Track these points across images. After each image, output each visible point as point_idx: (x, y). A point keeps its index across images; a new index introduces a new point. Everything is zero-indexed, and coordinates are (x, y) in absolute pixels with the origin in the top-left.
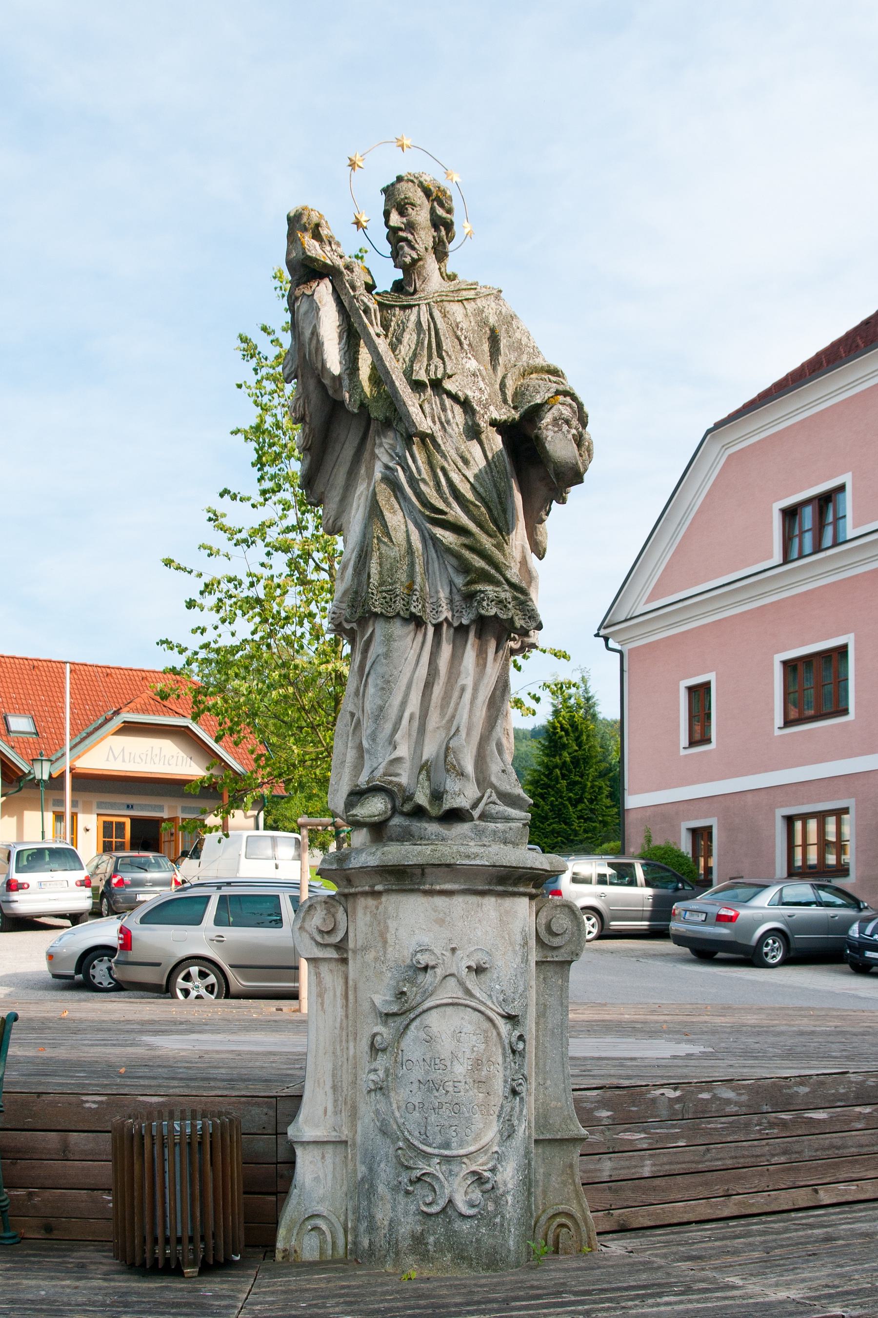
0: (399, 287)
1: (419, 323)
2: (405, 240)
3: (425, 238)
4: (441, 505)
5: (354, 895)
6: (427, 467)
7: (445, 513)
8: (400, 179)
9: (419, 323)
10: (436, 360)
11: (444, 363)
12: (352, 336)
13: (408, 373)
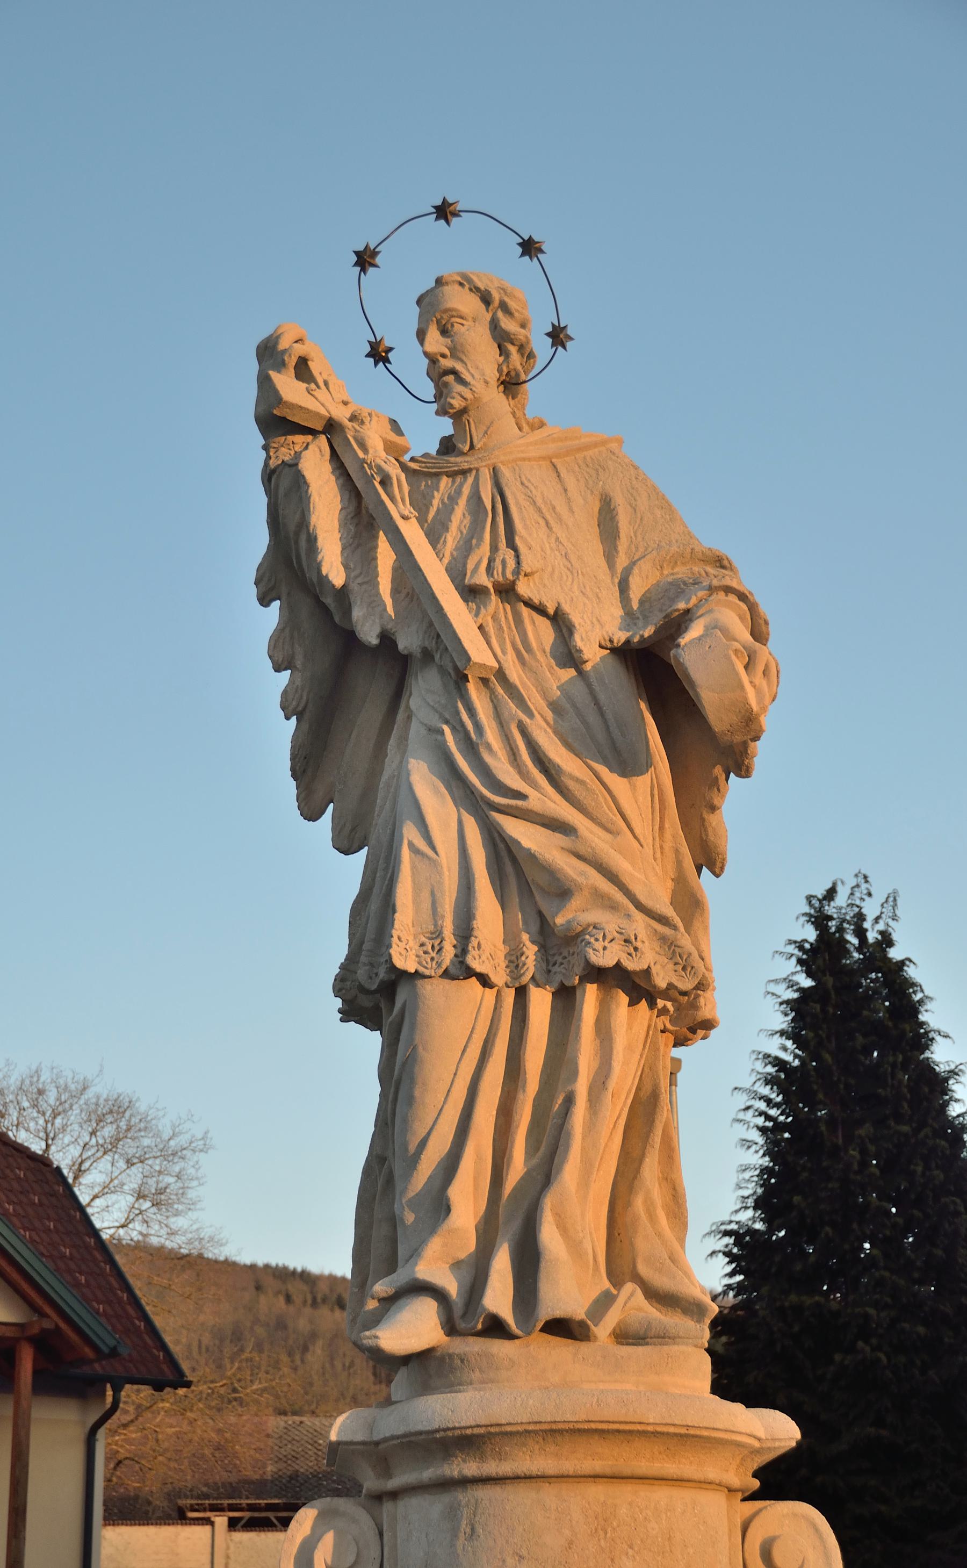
0: (448, 446)
1: (476, 497)
2: (453, 372)
3: (482, 363)
4: (512, 780)
5: (394, 1495)
6: (494, 724)
7: (522, 796)
8: (439, 282)
9: (476, 497)
10: (505, 553)
11: (517, 556)
12: (364, 519)
13: (457, 573)
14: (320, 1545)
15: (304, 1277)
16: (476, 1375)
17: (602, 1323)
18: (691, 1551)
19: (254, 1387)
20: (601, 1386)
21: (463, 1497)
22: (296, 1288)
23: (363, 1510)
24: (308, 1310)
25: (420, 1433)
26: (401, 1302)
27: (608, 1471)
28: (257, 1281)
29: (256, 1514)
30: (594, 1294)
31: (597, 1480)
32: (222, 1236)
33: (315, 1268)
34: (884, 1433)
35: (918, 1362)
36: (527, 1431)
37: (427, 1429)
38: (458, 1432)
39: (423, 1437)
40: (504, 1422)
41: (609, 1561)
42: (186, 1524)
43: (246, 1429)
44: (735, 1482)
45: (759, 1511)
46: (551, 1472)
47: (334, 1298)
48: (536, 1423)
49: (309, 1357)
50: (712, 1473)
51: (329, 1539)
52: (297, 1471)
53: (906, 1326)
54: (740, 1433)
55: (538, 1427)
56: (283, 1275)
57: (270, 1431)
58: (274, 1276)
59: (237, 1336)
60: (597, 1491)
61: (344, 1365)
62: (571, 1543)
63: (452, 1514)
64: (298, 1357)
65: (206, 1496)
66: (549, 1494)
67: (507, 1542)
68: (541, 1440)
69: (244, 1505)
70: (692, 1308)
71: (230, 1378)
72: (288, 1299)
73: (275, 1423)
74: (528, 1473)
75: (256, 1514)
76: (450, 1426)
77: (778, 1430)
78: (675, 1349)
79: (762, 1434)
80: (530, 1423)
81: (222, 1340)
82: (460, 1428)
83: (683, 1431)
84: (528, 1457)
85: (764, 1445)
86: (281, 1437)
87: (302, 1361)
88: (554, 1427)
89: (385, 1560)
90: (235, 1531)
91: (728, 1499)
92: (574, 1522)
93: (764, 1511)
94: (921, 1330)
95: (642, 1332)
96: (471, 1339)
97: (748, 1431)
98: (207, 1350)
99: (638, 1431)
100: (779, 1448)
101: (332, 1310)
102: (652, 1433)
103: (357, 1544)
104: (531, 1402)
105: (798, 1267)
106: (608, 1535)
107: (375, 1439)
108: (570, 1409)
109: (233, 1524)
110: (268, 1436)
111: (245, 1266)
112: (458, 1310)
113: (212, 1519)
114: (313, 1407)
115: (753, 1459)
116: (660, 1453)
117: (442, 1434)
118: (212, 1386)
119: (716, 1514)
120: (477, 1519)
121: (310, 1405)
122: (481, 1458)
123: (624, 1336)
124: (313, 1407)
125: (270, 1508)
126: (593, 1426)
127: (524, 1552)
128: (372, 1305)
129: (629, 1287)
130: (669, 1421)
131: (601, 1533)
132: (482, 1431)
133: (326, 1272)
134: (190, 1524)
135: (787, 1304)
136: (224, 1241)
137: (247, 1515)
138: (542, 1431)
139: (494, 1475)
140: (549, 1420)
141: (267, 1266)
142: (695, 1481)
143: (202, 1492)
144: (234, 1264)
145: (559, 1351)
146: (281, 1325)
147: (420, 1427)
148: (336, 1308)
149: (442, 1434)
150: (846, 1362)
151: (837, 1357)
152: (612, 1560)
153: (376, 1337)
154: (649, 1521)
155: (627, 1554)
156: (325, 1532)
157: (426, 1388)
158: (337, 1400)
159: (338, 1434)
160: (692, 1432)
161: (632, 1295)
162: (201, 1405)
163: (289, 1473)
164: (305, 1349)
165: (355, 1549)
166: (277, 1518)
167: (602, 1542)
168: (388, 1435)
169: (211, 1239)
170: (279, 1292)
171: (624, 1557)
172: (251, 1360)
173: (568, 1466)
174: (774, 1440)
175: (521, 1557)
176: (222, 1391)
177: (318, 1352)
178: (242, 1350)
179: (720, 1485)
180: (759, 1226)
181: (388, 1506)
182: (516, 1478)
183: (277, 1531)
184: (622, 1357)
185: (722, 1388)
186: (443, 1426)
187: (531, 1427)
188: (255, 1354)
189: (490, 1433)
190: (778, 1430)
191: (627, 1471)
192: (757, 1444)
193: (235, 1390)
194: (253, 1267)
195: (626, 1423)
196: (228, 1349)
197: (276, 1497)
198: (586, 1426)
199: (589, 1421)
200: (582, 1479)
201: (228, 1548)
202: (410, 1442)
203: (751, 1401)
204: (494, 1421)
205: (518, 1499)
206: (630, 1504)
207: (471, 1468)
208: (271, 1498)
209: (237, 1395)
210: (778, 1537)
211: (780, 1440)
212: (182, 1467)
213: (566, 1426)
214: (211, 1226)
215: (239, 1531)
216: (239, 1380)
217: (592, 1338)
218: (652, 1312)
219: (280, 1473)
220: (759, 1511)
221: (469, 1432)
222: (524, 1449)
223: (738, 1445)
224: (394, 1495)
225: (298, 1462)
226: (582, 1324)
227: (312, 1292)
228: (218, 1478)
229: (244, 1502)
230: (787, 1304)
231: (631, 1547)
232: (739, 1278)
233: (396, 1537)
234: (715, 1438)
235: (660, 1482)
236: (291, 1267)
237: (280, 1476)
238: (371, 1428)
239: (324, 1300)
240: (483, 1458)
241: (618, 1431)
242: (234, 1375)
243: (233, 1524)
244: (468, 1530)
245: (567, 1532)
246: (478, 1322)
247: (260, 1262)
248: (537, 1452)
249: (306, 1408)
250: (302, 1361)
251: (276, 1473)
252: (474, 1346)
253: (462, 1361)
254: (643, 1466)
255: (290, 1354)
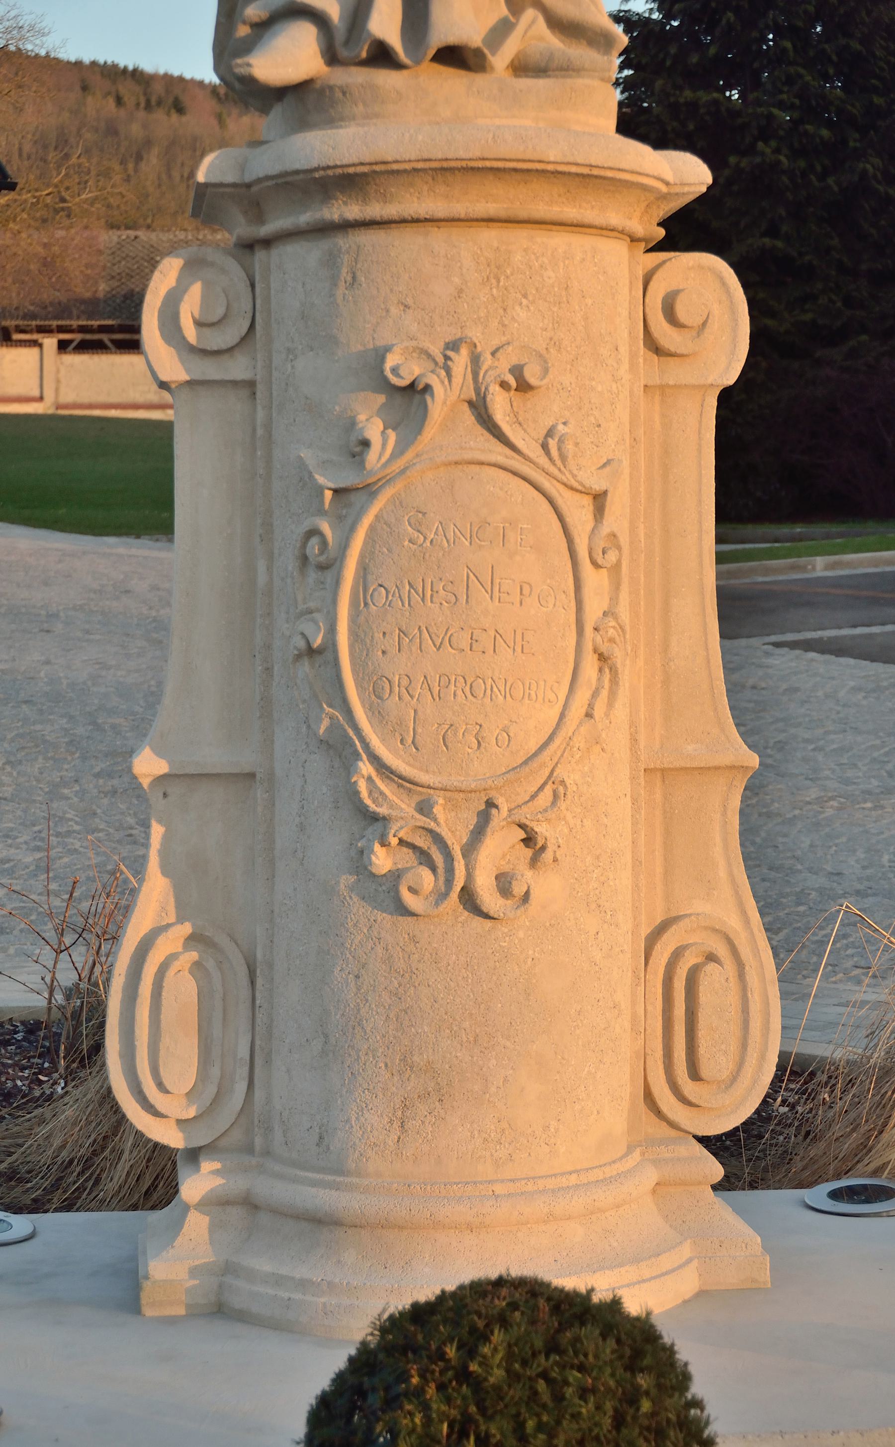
5: (267, 243)
14: (186, 297)
15: (136, 75)
16: (360, 109)
17: (499, 52)
18: (589, 301)
19: (83, 196)
20: (497, 122)
21: (343, 242)
22: (126, 89)
23: (233, 260)
24: (141, 114)
25: (297, 172)
26: (277, 27)
27: (503, 214)
28: (83, 81)
29: (88, 337)
30: (491, 20)
31: (490, 224)
32: (43, 24)
33: (148, 66)
34: (779, 244)
35: (819, 168)
36: (415, 170)
37: (306, 167)
38: (339, 171)
39: (301, 176)
40: (390, 159)
41: (501, 311)
42: (11, 346)
43: (75, 242)
44: (639, 229)
45: (664, 262)
46: (441, 214)
47: (170, 100)
48: (425, 160)
49: (143, 165)
50: (614, 219)
51: (196, 290)
52: (132, 290)
53: (809, 128)
54: (647, 175)
55: (427, 165)
56: (112, 73)
57: (102, 247)
58: (102, 74)
59: (62, 142)
60: (490, 236)
61: (182, 176)
62: (461, 291)
63: (331, 261)
64: (131, 166)
65: (34, 317)
66: (438, 238)
67: (391, 290)
68: (430, 179)
69: (75, 327)
70: (598, 40)
71: (56, 186)
72: (119, 101)
73: (107, 238)
74: (415, 216)
75: (88, 337)
76: (331, 164)
77: (687, 174)
78: (580, 82)
79: (670, 178)
80: (418, 161)
81: (45, 147)
82: (342, 166)
83: (586, 171)
84: (415, 200)
85: (672, 191)
86: (113, 253)
87: (136, 170)
88: (445, 165)
89: (257, 314)
90: (65, 353)
91: (630, 248)
92: (464, 270)
93: (668, 264)
94: (825, 133)
95: (543, 64)
96: (354, 70)
97: (656, 174)
98: (29, 158)
99: (537, 170)
100: (688, 193)
101: (168, 114)
102: (553, 173)
103: (227, 296)
104: (420, 138)
105: (694, 59)
106: (501, 284)
107: (248, 178)
108: (462, 145)
109: (63, 346)
110: (100, 252)
111: (68, 63)
112: (340, 35)
113: (40, 341)
114: (149, 221)
115: (659, 207)
116: (560, 196)
117: (322, 173)
118: (37, 194)
119: (619, 262)
120: (359, 266)
121: (145, 219)
122: (364, 201)
123: (522, 67)
124: (149, 221)
125: (102, 329)
126: (488, 164)
127: (409, 301)
128: (243, 31)
129: (530, 14)
130: (571, 160)
131: (494, 281)
132: (365, 169)
133: (162, 71)
134: (16, 346)
135: (682, 100)
136: (46, 31)
137: (78, 337)
138: (431, 169)
139: (378, 218)
140: (440, 157)
141: (94, 64)
142: (595, 227)
143: (29, 310)
144: (57, 61)
145: (452, 81)
146: (112, 130)
147: (297, 166)
148: (173, 111)
149: (322, 173)
150: (743, 165)
151: (733, 160)
152: (505, 310)
153: (249, 65)
154: (546, 269)
155: (521, 304)
156: (191, 283)
157: (302, 124)
158: (175, 213)
159: (206, 176)
160: (595, 172)
161: (533, 22)
162: (25, 216)
163: (123, 293)
164: (139, 158)
165: (225, 302)
166: (113, 341)
167: (494, 291)
168: (261, 175)
169: (32, 28)
170: (109, 93)
171: (517, 308)
172: (80, 166)
173: (459, 209)
174: (683, 184)
175: (407, 307)
176: (48, 200)
177: (153, 161)
178: (67, 156)
179: (622, 232)
180: (656, 16)
181: (260, 255)
182: (403, 221)
183: (111, 353)
184: (521, 91)
185: (630, 124)
186: (323, 164)
187: (420, 165)
188: (83, 160)
189: (375, 172)
190: (687, 174)
191: (523, 214)
192: (664, 189)
193: (63, 200)
194: (78, 64)
195: (524, 161)
196: (52, 156)
197: (109, 318)
198: (480, 164)
199: (484, 159)
200: (475, 223)
201: (58, 371)
202: (287, 183)
203: (659, 143)
204: (379, 158)
205: (403, 245)
206: (526, 250)
207: (353, 211)
208: (104, 319)
209: (65, 205)
210: (683, 290)
211: (689, 185)
212: (7, 285)
213: (458, 164)
214: (31, 14)
215: (70, 353)
216: (67, 188)
217: (488, 69)
218: (554, 42)
219: (114, 292)
220: (664, 262)
221: (351, 170)
222: (412, 190)
223: (645, 188)
224: (267, 243)
225: (133, 280)
226: (478, 53)
227: (145, 94)
228: (45, 296)
229: (75, 323)
230: (682, 100)
231: (525, 296)
232: (627, 72)
233: (269, 289)
234: (620, 180)
235: (558, 228)
236: (122, 65)
237: (114, 296)
238: (242, 168)
239: (159, 103)
240: (365, 200)
241: (515, 170)
242: (61, 181)
243: (63, 346)
244: (349, 279)
245: (456, 280)
246: (362, 49)
247: (87, 60)
248: (425, 193)
249: (141, 221)
250: (136, 170)
251: (109, 292)
252: (357, 77)
253: (344, 93)
254: (542, 209)
255: (123, 162)
